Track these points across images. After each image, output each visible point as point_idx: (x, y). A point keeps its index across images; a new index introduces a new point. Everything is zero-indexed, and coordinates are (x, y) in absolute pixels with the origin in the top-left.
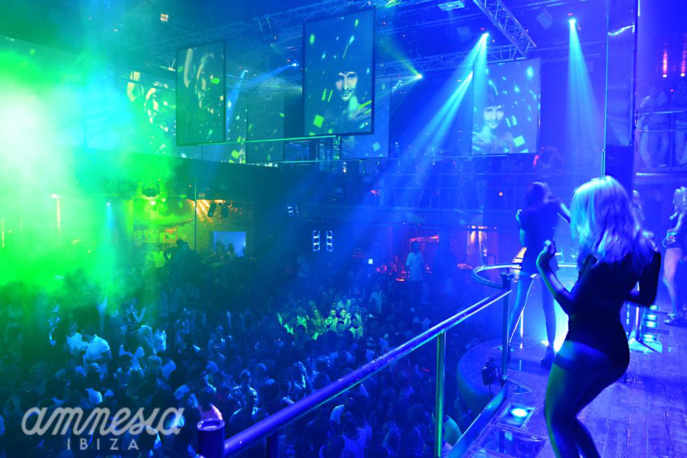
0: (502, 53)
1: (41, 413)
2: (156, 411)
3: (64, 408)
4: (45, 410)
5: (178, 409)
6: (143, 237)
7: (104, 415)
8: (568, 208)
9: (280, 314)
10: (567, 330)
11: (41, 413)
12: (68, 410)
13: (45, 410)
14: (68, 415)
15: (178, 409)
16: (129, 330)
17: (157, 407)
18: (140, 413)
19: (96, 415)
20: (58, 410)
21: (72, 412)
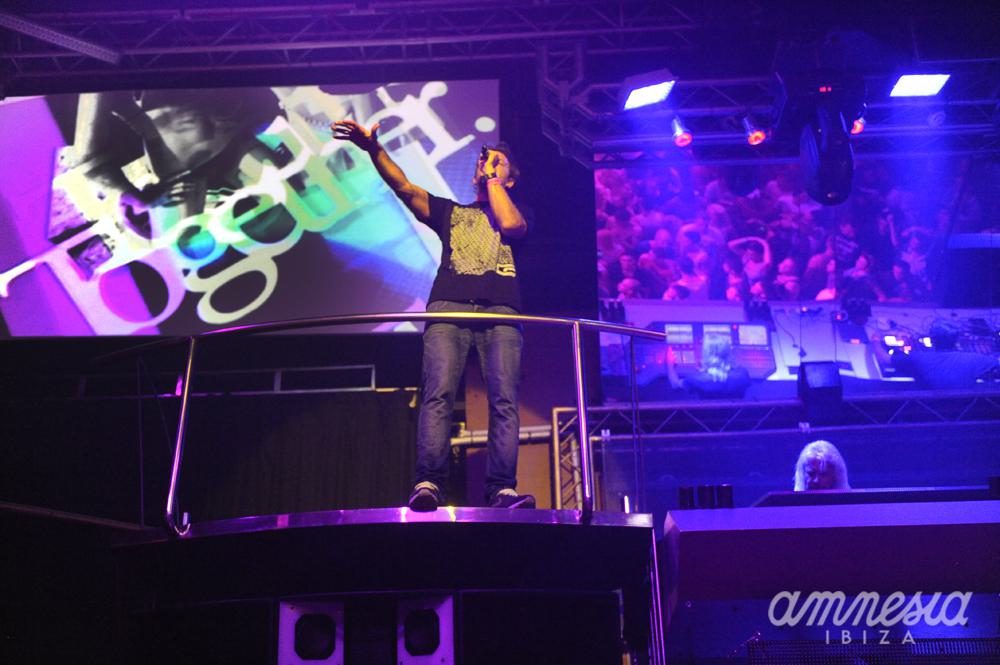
0: (283, 388)
1: (794, 598)
2: (937, 596)
3: (833, 592)
4: (797, 594)
5: (792, 593)
6: (269, 224)
7: (871, 601)
8: (516, 507)
9: (472, 143)
10: (440, 243)
11: (794, 598)
12: (827, 594)
13: (797, 594)
14: (826, 601)
15: (792, 593)
16: (717, 355)
17: (798, 590)
18: (917, 598)
19: (862, 600)
20: (815, 595)
21: (832, 597)
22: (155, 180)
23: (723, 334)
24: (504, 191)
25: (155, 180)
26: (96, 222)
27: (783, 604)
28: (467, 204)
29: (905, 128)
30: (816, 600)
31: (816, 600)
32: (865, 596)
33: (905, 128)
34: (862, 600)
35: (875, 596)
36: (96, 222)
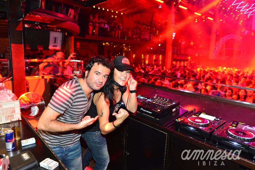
1: (189, 152)
2: (231, 151)
4: (190, 151)
5: (188, 150)
7: (212, 153)
11: (189, 152)
12: (198, 151)
13: (190, 151)
14: (198, 153)
15: (188, 150)
17: (190, 149)
19: (209, 153)
20: (195, 151)
22: (198, 79)
23: (53, 100)
24: (124, 101)
25: (198, 79)
26: (75, 84)
27: (186, 153)
28: (93, 100)
29: (182, 107)
30: (195, 152)
31: (195, 152)
32: (210, 151)
33: (182, 107)
34: (209, 153)
35: (213, 151)
36: (75, 84)
